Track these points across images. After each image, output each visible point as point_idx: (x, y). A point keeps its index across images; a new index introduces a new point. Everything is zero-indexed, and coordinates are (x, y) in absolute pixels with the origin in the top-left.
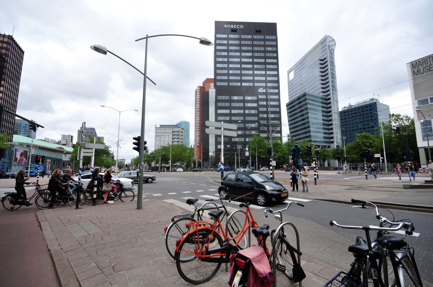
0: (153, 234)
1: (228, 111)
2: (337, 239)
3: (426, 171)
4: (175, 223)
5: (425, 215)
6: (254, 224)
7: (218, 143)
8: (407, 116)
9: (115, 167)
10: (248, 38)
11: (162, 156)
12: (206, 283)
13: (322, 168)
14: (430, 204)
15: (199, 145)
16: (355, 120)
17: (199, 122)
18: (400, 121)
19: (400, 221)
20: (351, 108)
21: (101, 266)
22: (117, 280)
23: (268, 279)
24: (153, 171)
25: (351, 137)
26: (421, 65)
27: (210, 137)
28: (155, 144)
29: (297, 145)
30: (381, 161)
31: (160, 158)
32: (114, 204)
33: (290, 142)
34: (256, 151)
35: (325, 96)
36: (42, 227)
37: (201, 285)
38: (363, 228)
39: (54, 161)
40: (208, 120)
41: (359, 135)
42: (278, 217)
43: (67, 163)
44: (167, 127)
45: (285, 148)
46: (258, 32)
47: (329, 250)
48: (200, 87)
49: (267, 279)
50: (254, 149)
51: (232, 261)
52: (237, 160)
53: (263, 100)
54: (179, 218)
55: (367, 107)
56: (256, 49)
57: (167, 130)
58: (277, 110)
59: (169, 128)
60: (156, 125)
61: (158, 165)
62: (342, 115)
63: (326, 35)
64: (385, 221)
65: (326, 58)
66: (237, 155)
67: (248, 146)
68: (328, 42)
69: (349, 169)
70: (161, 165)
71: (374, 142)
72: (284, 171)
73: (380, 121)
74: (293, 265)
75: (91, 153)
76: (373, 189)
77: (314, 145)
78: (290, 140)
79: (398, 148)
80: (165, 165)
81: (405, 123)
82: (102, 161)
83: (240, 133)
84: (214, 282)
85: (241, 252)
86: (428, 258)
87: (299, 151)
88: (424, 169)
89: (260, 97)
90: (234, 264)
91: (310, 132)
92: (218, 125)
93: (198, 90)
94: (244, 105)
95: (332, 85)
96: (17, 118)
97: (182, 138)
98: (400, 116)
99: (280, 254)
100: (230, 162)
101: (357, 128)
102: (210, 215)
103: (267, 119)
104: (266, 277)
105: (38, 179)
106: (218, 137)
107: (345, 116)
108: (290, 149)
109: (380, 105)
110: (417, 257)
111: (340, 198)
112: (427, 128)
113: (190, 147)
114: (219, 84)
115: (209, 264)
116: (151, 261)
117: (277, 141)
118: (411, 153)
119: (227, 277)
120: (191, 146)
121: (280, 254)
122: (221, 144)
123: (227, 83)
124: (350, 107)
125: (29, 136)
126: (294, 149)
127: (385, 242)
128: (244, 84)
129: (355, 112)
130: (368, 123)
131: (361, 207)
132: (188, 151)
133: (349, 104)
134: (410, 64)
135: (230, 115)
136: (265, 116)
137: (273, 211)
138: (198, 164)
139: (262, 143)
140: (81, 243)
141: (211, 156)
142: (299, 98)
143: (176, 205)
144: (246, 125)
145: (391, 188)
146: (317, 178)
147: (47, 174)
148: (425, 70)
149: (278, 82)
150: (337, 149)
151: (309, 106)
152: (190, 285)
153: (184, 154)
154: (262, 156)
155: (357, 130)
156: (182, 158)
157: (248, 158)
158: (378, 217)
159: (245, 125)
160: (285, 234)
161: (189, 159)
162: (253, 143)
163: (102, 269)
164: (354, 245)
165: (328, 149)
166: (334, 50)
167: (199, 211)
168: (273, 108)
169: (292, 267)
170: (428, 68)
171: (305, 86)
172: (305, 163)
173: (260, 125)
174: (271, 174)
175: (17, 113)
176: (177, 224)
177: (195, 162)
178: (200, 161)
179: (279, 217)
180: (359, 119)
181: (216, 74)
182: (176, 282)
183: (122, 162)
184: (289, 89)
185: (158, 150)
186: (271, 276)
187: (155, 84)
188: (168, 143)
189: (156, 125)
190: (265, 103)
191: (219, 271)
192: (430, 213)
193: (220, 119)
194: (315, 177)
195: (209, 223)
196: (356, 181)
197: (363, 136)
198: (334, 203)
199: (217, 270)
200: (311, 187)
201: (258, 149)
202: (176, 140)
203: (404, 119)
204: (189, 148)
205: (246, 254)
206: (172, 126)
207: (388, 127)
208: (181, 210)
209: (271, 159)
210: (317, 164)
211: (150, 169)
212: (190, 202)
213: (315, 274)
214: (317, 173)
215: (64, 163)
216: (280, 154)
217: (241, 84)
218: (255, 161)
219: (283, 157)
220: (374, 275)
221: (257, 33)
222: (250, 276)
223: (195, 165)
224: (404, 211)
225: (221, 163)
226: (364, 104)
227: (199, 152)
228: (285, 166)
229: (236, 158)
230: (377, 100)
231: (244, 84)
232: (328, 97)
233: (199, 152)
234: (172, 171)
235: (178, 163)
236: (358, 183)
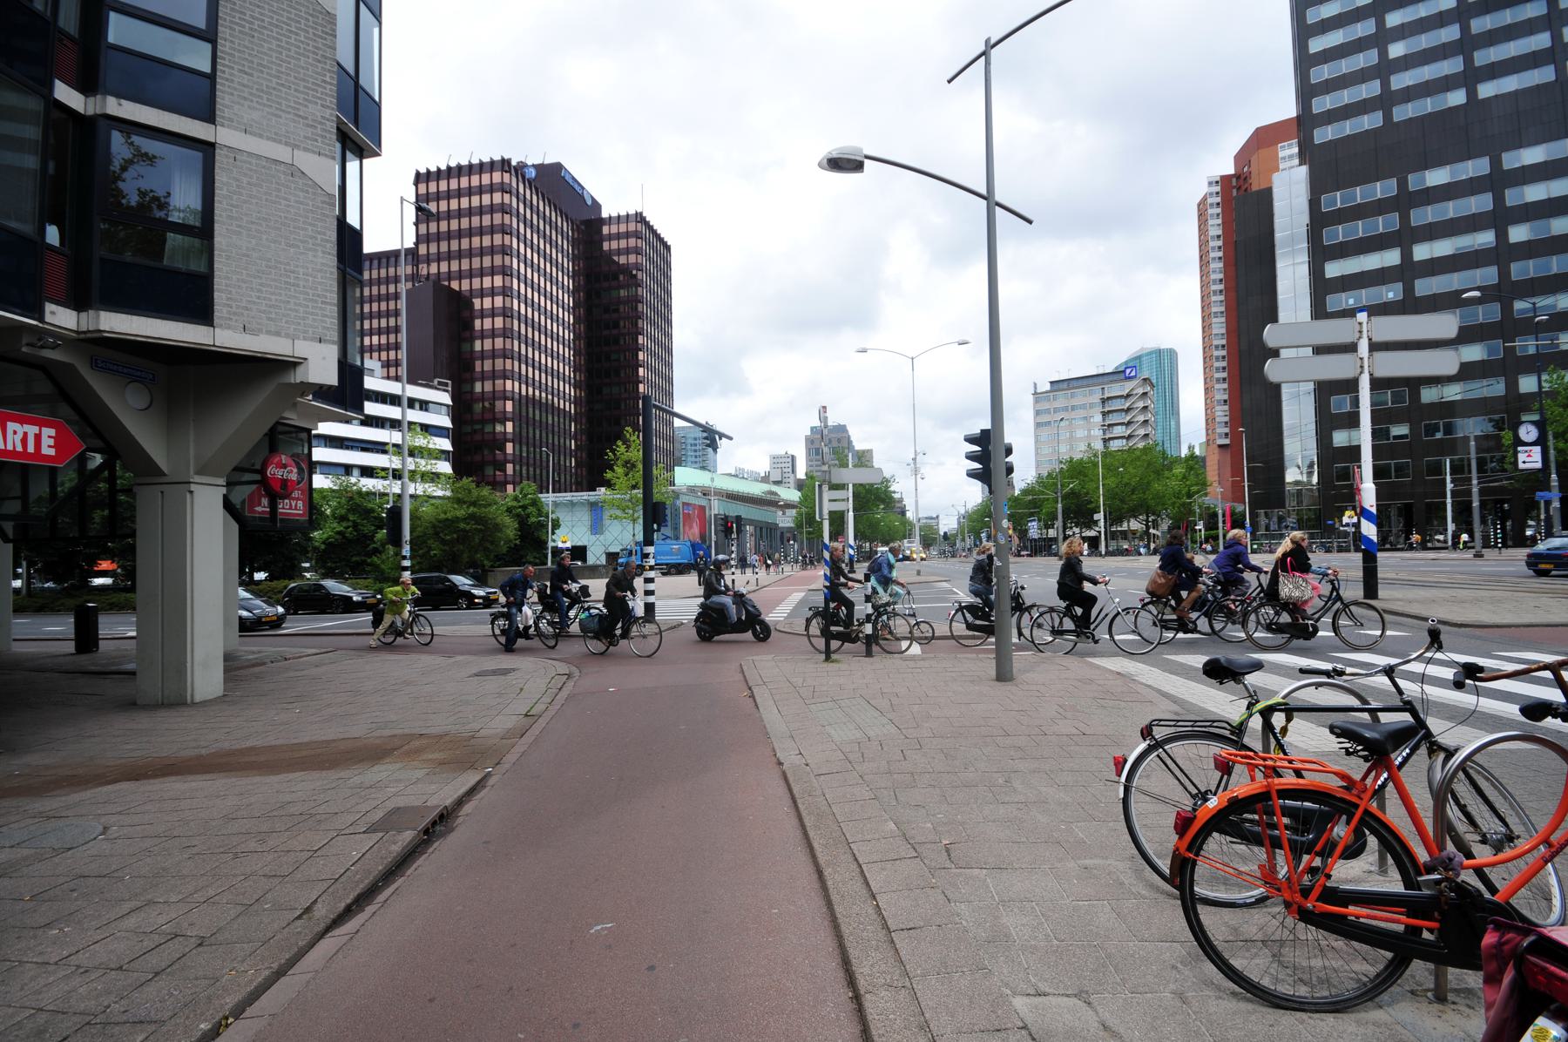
0: (1062, 770)
9: (912, 542)
12: (1330, 1019)
15: (1227, 441)
21: (913, 838)
22: (963, 891)
24: (1036, 555)
27: (1285, 397)
28: (1037, 454)
31: (1060, 505)
32: (924, 656)
36: (758, 700)
39: (761, 529)
40: (1274, 319)
43: (788, 535)
44: (1080, 383)
48: (1225, 180)
51: (1494, 965)
54: (1173, 730)
60: (1035, 384)
61: (1052, 533)
67: (1536, 417)
70: (1064, 531)
75: (843, 500)
82: (874, 525)
83: (1474, 353)
90: (1514, 984)
93: (1210, 200)
96: (678, 423)
102: (1338, 736)
105: (733, 577)
115: (1340, 943)
120: (1191, 448)
125: (703, 468)
128: (1486, 90)
132: (1179, 470)
140: (851, 757)
141: (1297, 483)
143: (1144, 681)
147: (750, 566)
156: (1152, 503)
157: (1537, 479)
161: (1183, 505)
163: (917, 846)
167: (1267, 713)
175: (677, 409)
176: (1164, 750)
177: (1215, 515)
181: (1306, 91)
183: (930, 527)
187: (1030, 222)
189: (1035, 384)
202: (1119, 431)
206: (1101, 380)
208: (1168, 702)
211: (1025, 548)
215: (782, 533)
225: (1363, 513)
227: (1229, 469)
229: (1449, 486)
231: (1486, 90)
234: (1109, 554)
235: (1132, 520)
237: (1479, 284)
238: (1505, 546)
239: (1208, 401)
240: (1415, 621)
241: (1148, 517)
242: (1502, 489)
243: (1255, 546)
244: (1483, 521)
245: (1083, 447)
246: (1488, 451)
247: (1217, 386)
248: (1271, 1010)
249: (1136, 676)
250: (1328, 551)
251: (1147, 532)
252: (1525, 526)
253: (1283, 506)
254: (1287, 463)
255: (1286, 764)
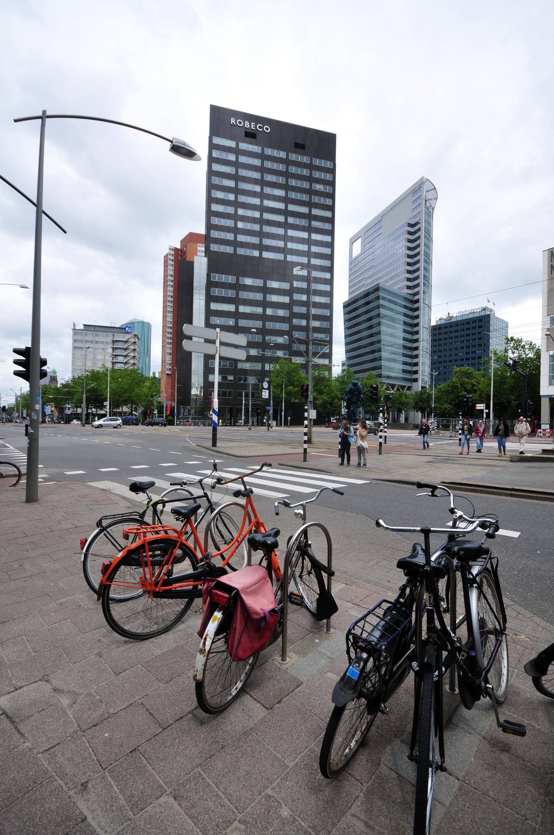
1: (231, 308)
2: (399, 545)
3: (547, 434)
4: (104, 529)
5: (532, 503)
6: (259, 526)
7: (208, 370)
8: (531, 343)
10: (278, 156)
11: (88, 391)
12: (163, 636)
13: (395, 424)
14: (542, 487)
15: (170, 372)
16: (455, 343)
17: (171, 326)
18: (521, 350)
19: (483, 516)
20: (449, 321)
25: (445, 373)
27: (193, 357)
28: (73, 364)
29: (357, 381)
31: (84, 396)
33: (345, 375)
35: (410, 294)
37: (153, 639)
38: (422, 531)
41: (458, 369)
42: (299, 514)
45: (335, 385)
46: (299, 147)
47: (385, 563)
48: (176, 250)
49: (266, 621)
50: (280, 386)
51: (206, 596)
52: (247, 405)
53: (300, 291)
54: (112, 520)
55: (475, 321)
56: (293, 182)
58: (326, 312)
59: (105, 332)
61: (79, 410)
62: (435, 332)
63: (423, 177)
64: (461, 517)
65: (419, 222)
66: (247, 396)
68: (425, 192)
69: (436, 428)
70: (87, 410)
71: (478, 383)
72: (330, 430)
73: (491, 348)
74: (319, 592)
76: (466, 462)
77: (385, 383)
78: (345, 373)
80: (96, 412)
81: (527, 353)
83: (253, 352)
84: (178, 633)
85: (223, 579)
86: (526, 571)
87: (360, 393)
88: (544, 430)
89: (296, 284)
90: (210, 601)
91: (381, 360)
92: (210, 333)
93: (170, 257)
94: (265, 297)
95: (425, 276)
97: (134, 357)
98: (521, 341)
99: (301, 577)
101: (456, 358)
102: (173, 513)
103: (306, 329)
104: (264, 618)
106: (209, 358)
107: (439, 334)
108: (344, 389)
109: (495, 321)
110: (511, 569)
111: (414, 477)
113: (151, 375)
114: (214, 247)
116: (53, 605)
117: (322, 372)
118: (529, 405)
119: (198, 622)
120: (154, 373)
121: (301, 577)
122: (213, 373)
124: (449, 319)
126: (351, 389)
127: (454, 551)
128: (266, 255)
129: (457, 328)
130: (474, 349)
131: (431, 494)
132: (148, 384)
133: (449, 314)
134: (549, 252)
135: (236, 315)
136: (304, 323)
137: (290, 504)
141: (196, 395)
142: (367, 295)
143: (116, 492)
144: (267, 338)
145: (492, 461)
146: (383, 442)
150: (421, 393)
151: (382, 311)
152: (132, 642)
153: (137, 390)
154: (293, 400)
155: (456, 360)
156: (134, 398)
157: (267, 402)
158: (452, 511)
159: (264, 338)
160: (310, 542)
161: (149, 400)
162: (278, 374)
164: (405, 558)
165: (408, 392)
166: (433, 209)
168: (318, 309)
169: (318, 596)
172: (368, 416)
173: (292, 340)
174: (305, 434)
176: (107, 532)
178: (173, 405)
179: (301, 514)
180: (461, 342)
181: (209, 226)
182: (102, 639)
184: (350, 275)
187: (65, 232)
188: (104, 366)
190: (304, 298)
191: (189, 612)
192: (540, 500)
194: (381, 440)
196: (443, 448)
197: (463, 372)
198: (405, 486)
199: (185, 611)
200: (371, 459)
201: (286, 386)
203: (527, 347)
205: (231, 581)
206: (112, 330)
207: (502, 359)
208: (125, 502)
209: (307, 406)
210: (386, 418)
212: (136, 488)
213: (354, 604)
214: (385, 434)
216: (326, 398)
217: (261, 254)
218: (279, 408)
219: (331, 404)
220: (428, 603)
221: (297, 149)
222: (237, 619)
224: (504, 497)
225: (214, 411)
226: (471, 316)
228: (333, 420)
229: (244, 402)
230: (491, 310)
231: (266, 255)
232: (416, 298)
235: (125, 406)
238: (258, 425)
239: (163, 352)
240: (227, 456)
241: (132, 405)
243: (178, 422)
244: (252, 416)
245: (100, 364)
247: (168, 346)
249: (113, 490)
250: (205, 425)
252: (263, 418)
254: (192, 386)
255: (161, 529)
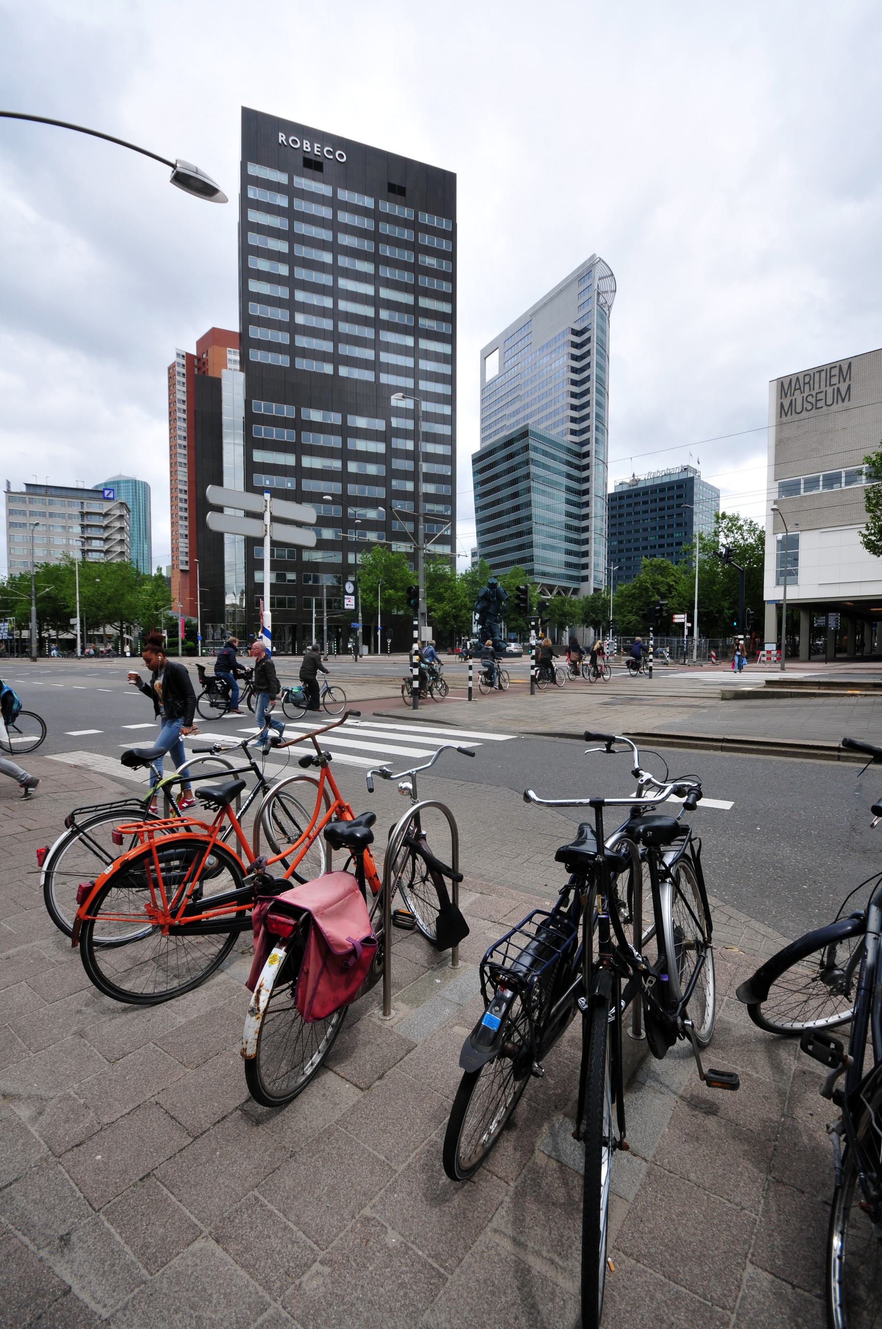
1: (289, 460)
6: (343, 812)
7: (253, 564)
12: (189, 995)
14: (764, 735)
15: (187, 568)
16: (643, 520)
17: (186, 488)
19: (680, 779)
23: (358, 955)
25: (629, 568)
26: (800, 388)
27: (226, 541)
29: (495, 581)
30: (686, 633)
31: (33, 608)
33: (477, 571)
34: (376, 595)
35: (576, 443)
37: (172, 1002)
38: (592, 804)
42: (406, 789)
46: (396, 191)
48: (188, 357)
50: (373, 590)
51: (258, 925)
52: (319, 621)
57: (58, 506)
58: (445, 470)
59: (67, 497)
61: (25, 634)
62: (615, 504)
63: (594, 255)
64: (649, 781)
68: (597, 278)
70: (40, 633)
73: (696, 529)
77: (538, 583)
78: (477, 567)
79: (725, 600)
80: (57, 635)
83: (328, 534)
84: (214, 988)
85: (286, 897)
87: (500, 599)
89: (395, 422)
90: (264, 932)
92: (254, 502)
94: (344, 443)
95: (598, 416)
98: (737, 519)
100: (294, 627)
102: (199, 797)
103: (413, 496)
104: (354, 952)
106: (252, 543)
112: (788, 555)
114: (257, 356)
117: (440, 567)
120: (159, 569)
121: (411, 886)
122: (262, 568)
123: (287, 358)
124: (634, 483)
126: (486, 593)
130: (670, 531)
132: (148, 587)
133: (634, 476)
137: (391, 774)
138: (186, 631)
139: (396, 573)
141: (233, 605)
142: (509, 442)
143: (99, 770)
144: (350, 511)
148: (806, 405)
149: (451, 380)
150: (593, 598)
151: (534, 469)
154: (395, 612)
155: (645, 548)
156: (126, 612)
158: (636, 774)
159: (345, 511)
160: (424, 832)
161: (152, 615)
162: (371, 569)
165: (574, 598)
166: (610, 307)
170: (813, 400)
171: (527, 406)
172: (513, 636)
173: (391, 515)
176: (85, 834)
177: (177, 625)
181: (246, 319)
185: (22, 576)
186: (369, 947)
190: (410, 445)
193: (263, 485)
195: (198, 821)
197: (655, 566)
198: (569, 741)
204: (151, 575)
206: (80, 494)
207: (710, 547)
219: (456, 617)
221: (392, 195)
223: (173, 633)
224: (712, 752)
225: (265, 631)
226: (666, 480)
227: (188, 590)
229: (314, 615)
230: (695, 471)
231: (343, 371)
233: (188, 591)
236: (631, 689)
237: (333, 492)
238: (338, 653)
241: (122, 624)
242: (338, 620)
244: (329, 639)
246: (333, 595)
247: (181, 522)
248: (149, 1009)
251: (120, 637)
252: (347, 642)
253: (224, 623)
254: (226, 590)
255: (179, 823)
